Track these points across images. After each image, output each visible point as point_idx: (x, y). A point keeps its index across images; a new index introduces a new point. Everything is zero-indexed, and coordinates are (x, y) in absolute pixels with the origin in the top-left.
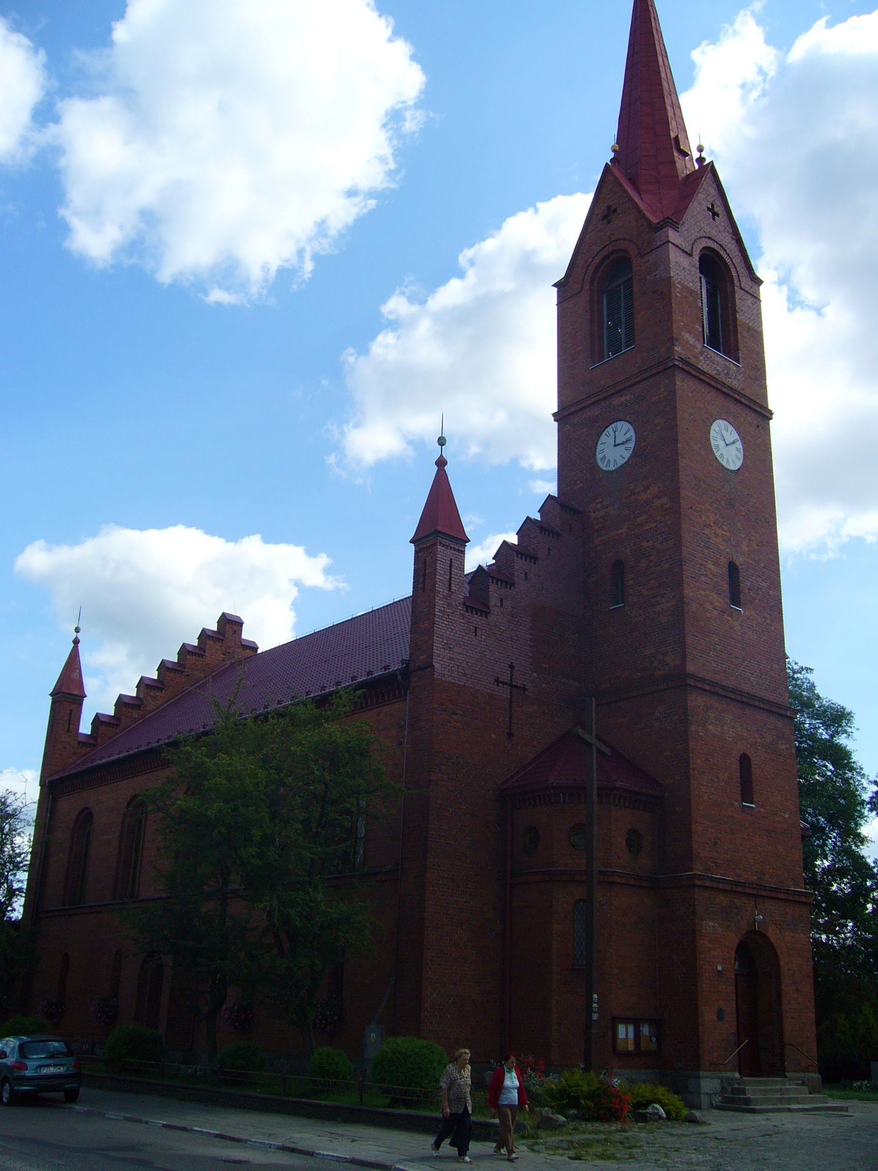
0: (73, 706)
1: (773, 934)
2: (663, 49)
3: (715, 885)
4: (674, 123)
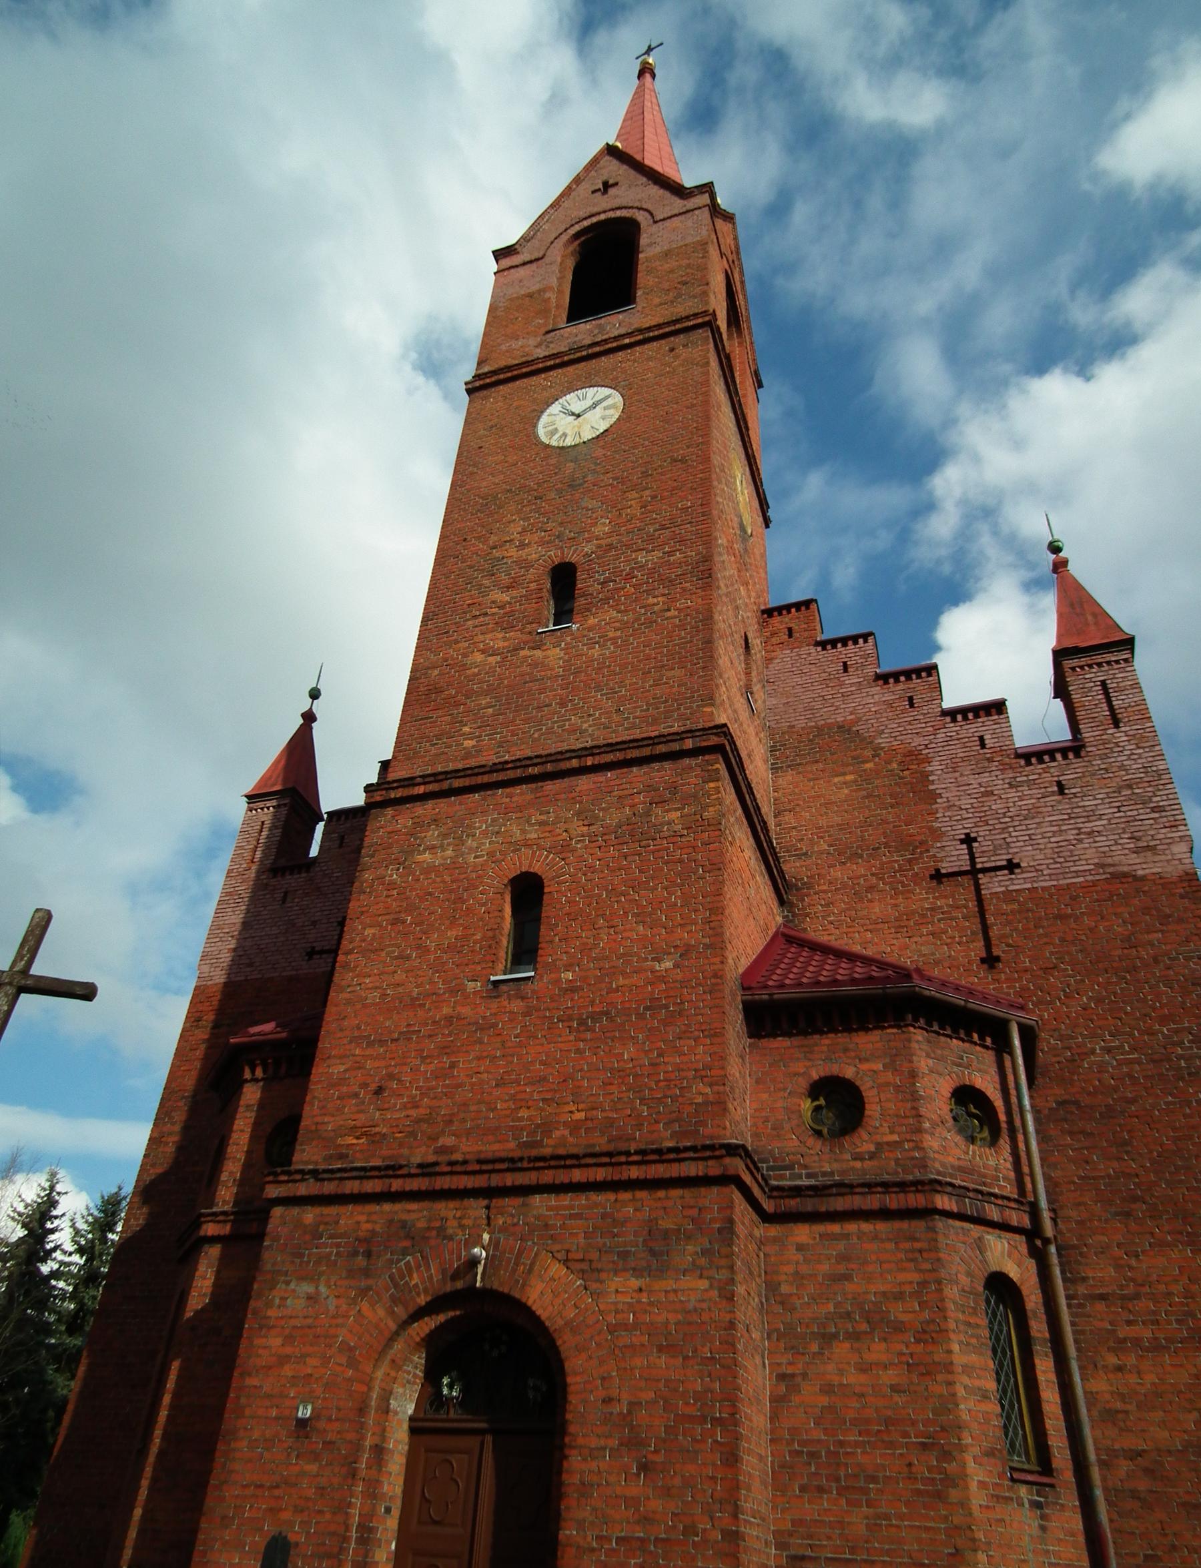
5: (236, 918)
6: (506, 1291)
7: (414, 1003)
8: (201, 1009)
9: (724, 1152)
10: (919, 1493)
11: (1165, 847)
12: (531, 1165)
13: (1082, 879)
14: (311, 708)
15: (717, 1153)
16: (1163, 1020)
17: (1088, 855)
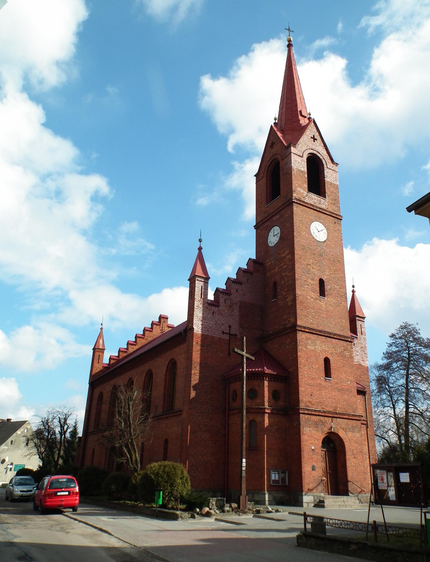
0: (100, 353)
1: (342, 434)
2: (297, 76)
3: (310, 412)
4: (300, 105)
14: (200, 246)
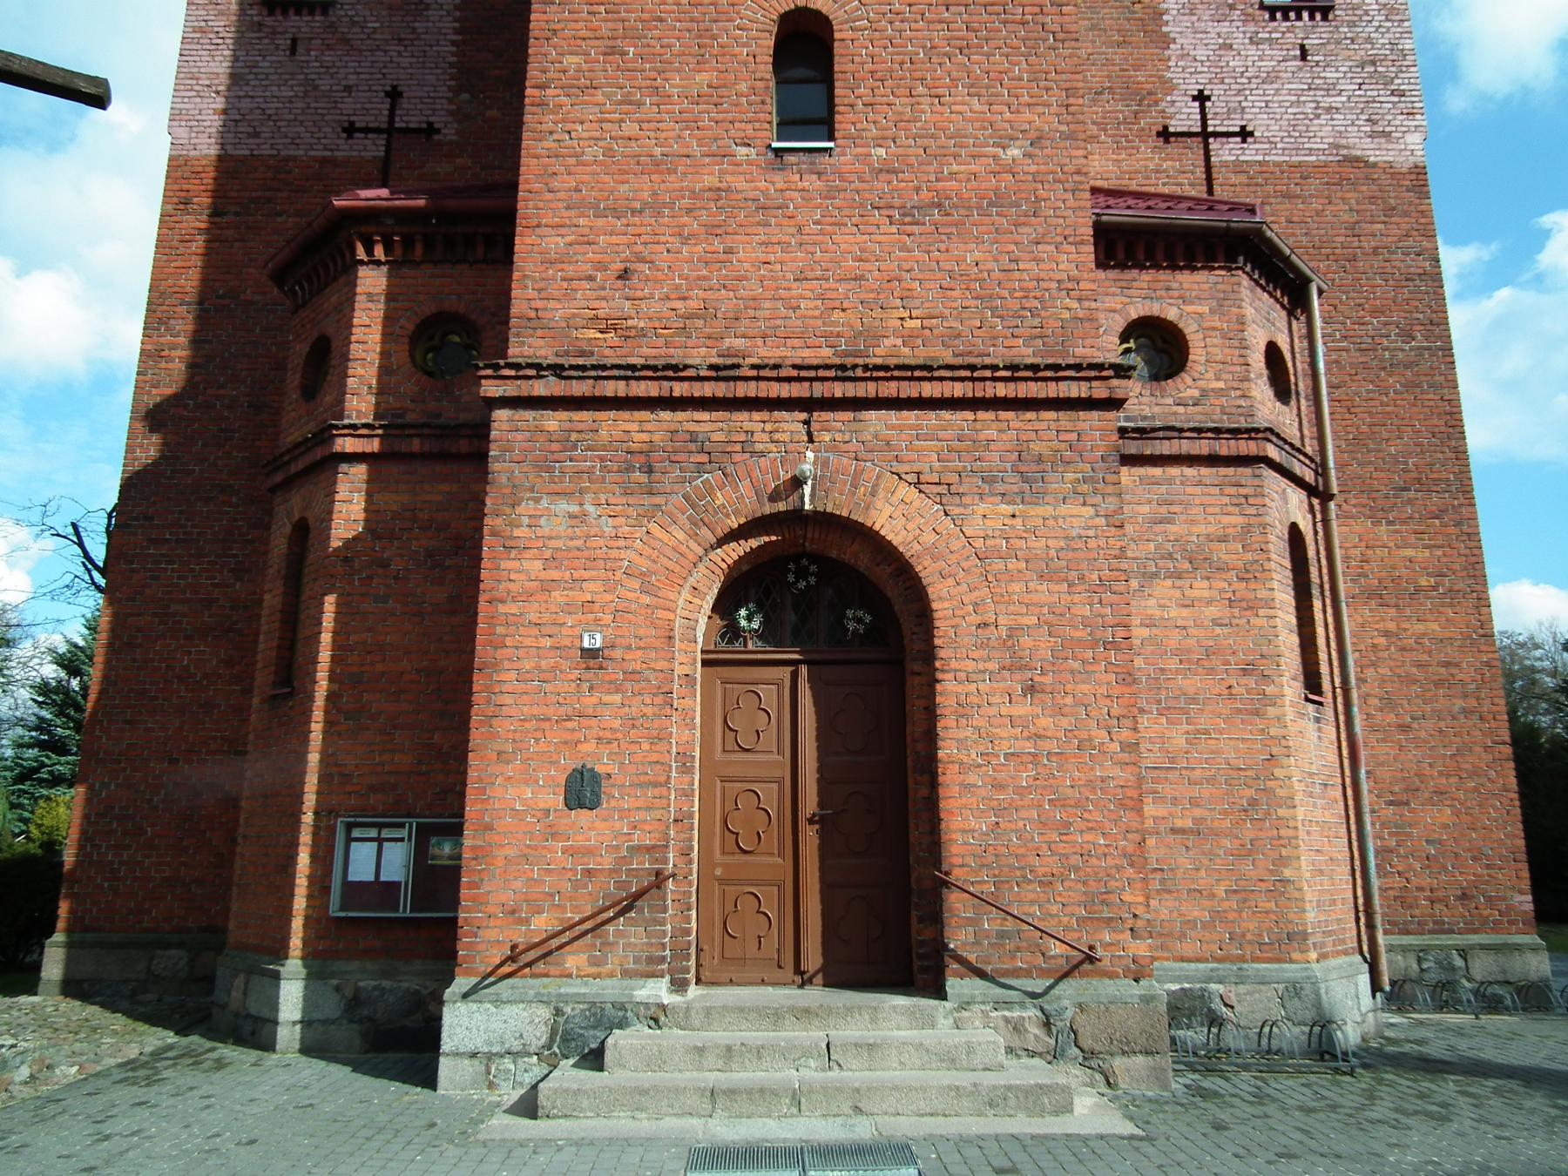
5: (219, 65)
6: (845, 514)
7: (658, 166)
8: (185, 187)
9: (1111, 373)
10: (1239, 711)
11: (1400, 135)
12: (868, 374)
13: (1313, 158)
15: (1105, 373)
16: (1375, 312)
17: (1323, 134)
